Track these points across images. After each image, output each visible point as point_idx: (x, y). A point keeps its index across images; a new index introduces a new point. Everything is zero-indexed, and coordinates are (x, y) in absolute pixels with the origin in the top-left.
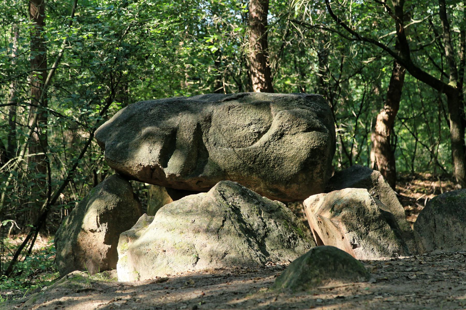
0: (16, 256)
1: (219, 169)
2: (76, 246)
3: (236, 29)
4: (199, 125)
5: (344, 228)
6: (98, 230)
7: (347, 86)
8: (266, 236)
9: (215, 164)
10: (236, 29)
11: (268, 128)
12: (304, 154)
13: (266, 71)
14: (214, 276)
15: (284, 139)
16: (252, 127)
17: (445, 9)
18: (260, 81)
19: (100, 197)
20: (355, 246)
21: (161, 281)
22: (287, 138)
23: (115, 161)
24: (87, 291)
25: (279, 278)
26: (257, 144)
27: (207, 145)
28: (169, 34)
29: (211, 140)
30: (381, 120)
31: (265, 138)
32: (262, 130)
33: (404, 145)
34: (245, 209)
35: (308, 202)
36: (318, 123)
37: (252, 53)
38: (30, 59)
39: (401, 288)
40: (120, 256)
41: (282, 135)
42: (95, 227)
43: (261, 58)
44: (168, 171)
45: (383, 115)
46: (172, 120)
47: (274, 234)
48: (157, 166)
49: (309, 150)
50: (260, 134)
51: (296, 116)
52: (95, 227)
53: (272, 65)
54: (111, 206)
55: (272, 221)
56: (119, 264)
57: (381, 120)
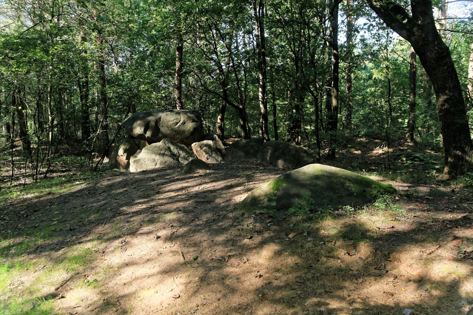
0: (97, 165)
1: (164, 135)
2: (116, 161)
3: (171, 89)
5: (204, 153)
7: (209, 108)
8: (179, 156)
9: (162, 133)
10: (171, 89)
12: (192, 130)
13: (181, 103)
14: (161, 169)
17: (312, 95)
18: (179, 106)
20: (208, 159)
21: (144, 171)
22: (186, 124)
24: (118, 175)
25: (182, 170)
26: (176, 126)
28: (148, 90)
29: (161, 125)
31: (179, 124)
33: (228, 127)
34: (172, 148)
35: (193, 145)
36: (196, 119)
37: (176, 96)
39: (220, 172)
40: (131, 164)
42: (122, 154)
43: (179, 98)
45: (219, 117)
46: (148, 118)
48: (143, 134)
50: (177, 123)
52: (122, 154)
53: (183, 101)
56: (130, 167)
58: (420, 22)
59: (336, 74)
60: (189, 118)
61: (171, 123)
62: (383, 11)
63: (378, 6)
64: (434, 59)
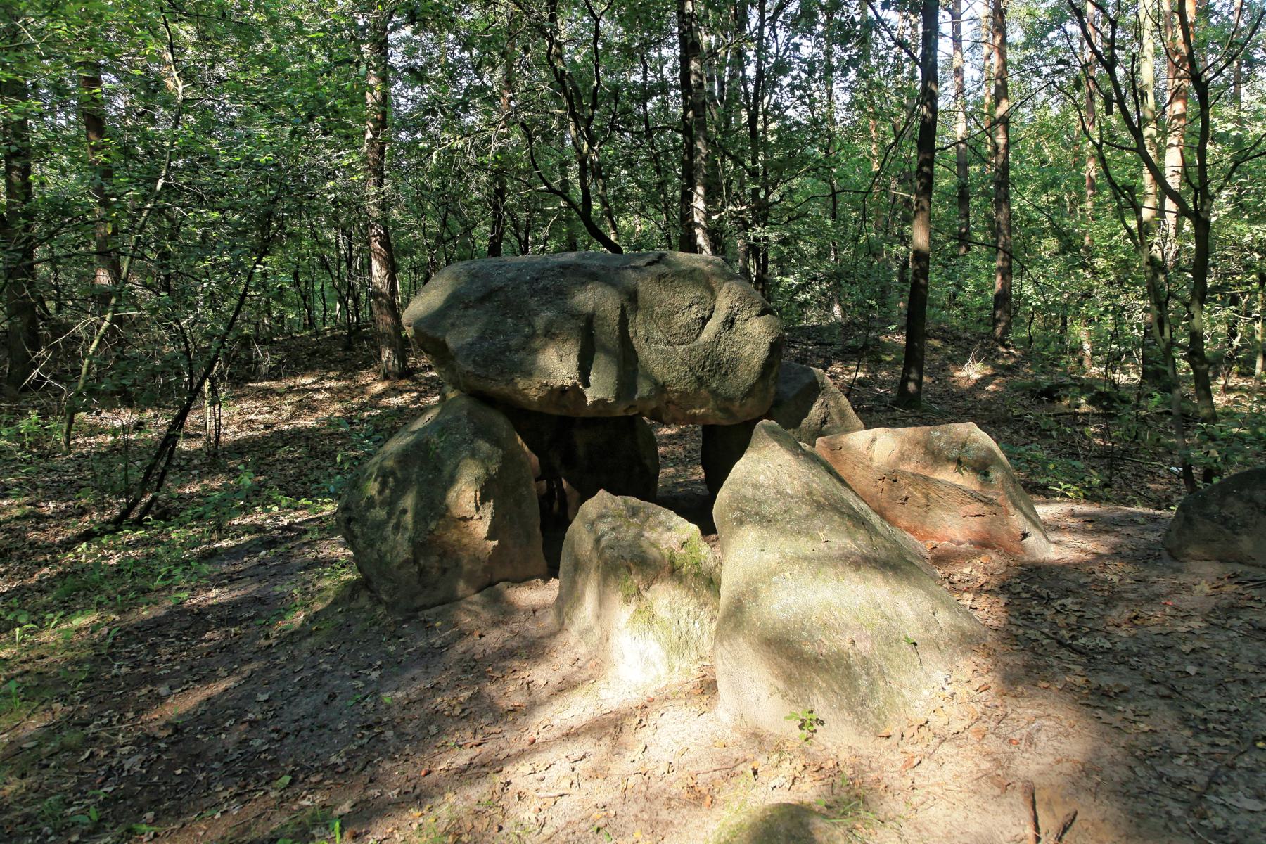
6: (477, 517)
15: (735, 327)
16: (694, 309)
23: (486, 377)
27: (634, 342)
29: (641, 332)
30: (944, 35)
32: (707, 313)
41: (733, 321)
48: (575, 386)
49: (768, 345)
50: (704, 320)
55: (104, 414)
57: (944, 35)
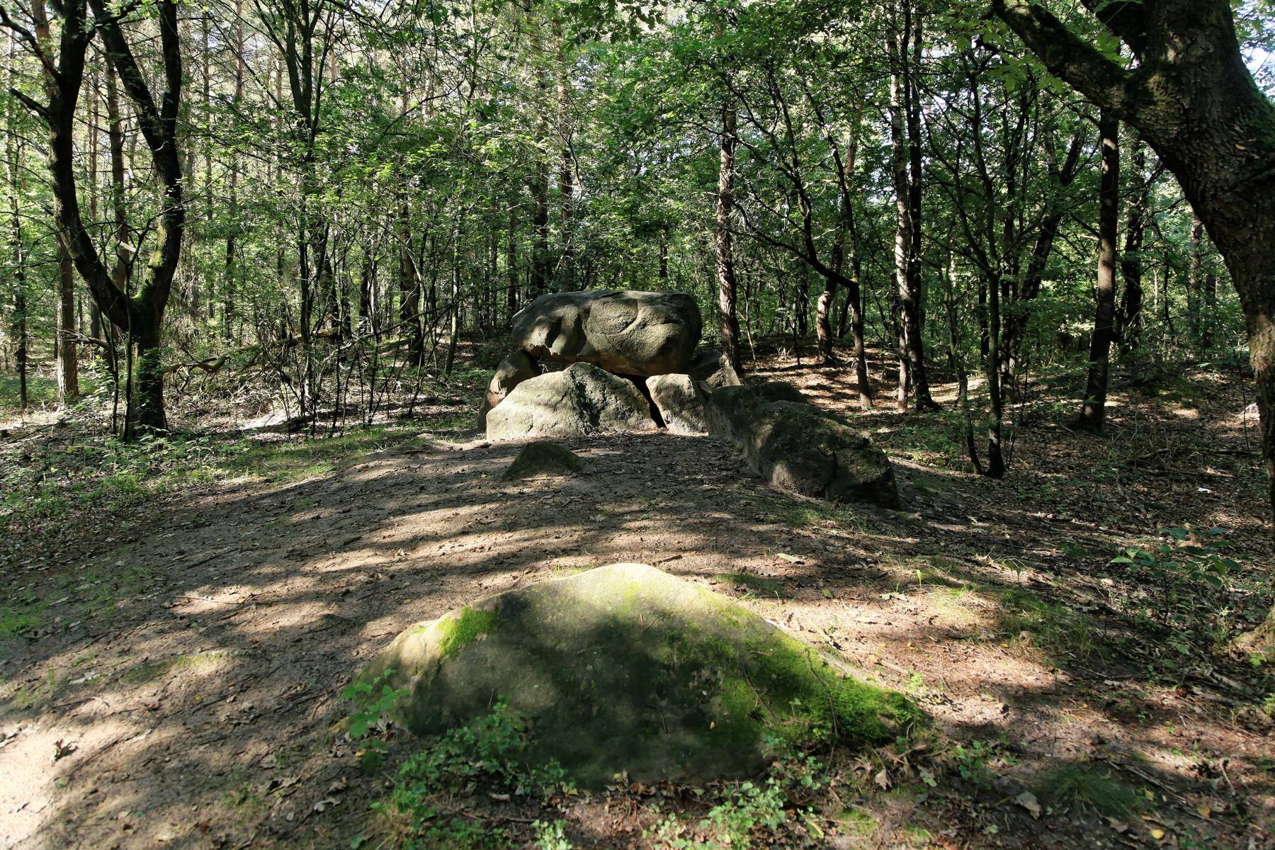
4: (579, 316)
8: (603, 408)
11: (634, 320)
12: (661, 341)
19: (504, 368)
22: (649, 328)
31: (631, 327)
34: (590, 385)
36: (675, 317)
38: (583, 247)
41: (645, 325)
44: (552, 350)
45: (823, 298)
47: (611, 408)
50: (627, 324)
51: (657, 311)
54: (510, 375)
58: (1171, 55)
59: (1109, 202)
60: (656, 312)
61: (612, 322)
62: (1037, 24)
63: (1022, 11)
64: (1231, 189)
